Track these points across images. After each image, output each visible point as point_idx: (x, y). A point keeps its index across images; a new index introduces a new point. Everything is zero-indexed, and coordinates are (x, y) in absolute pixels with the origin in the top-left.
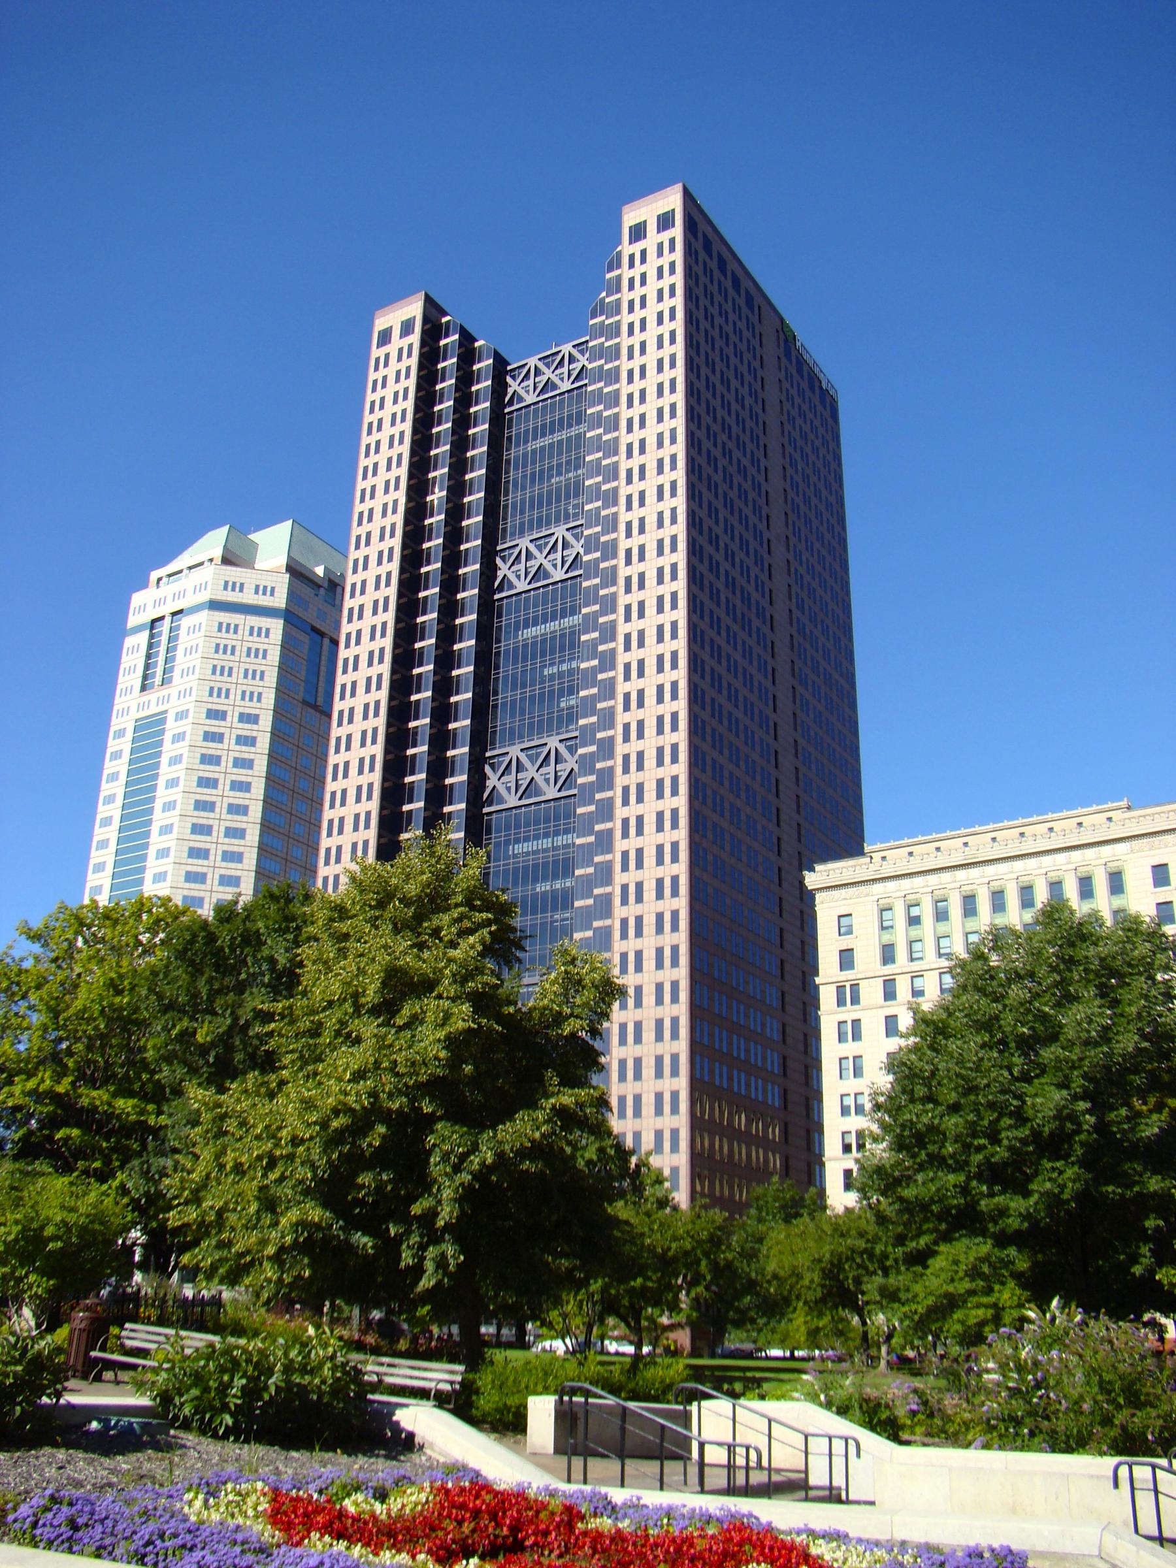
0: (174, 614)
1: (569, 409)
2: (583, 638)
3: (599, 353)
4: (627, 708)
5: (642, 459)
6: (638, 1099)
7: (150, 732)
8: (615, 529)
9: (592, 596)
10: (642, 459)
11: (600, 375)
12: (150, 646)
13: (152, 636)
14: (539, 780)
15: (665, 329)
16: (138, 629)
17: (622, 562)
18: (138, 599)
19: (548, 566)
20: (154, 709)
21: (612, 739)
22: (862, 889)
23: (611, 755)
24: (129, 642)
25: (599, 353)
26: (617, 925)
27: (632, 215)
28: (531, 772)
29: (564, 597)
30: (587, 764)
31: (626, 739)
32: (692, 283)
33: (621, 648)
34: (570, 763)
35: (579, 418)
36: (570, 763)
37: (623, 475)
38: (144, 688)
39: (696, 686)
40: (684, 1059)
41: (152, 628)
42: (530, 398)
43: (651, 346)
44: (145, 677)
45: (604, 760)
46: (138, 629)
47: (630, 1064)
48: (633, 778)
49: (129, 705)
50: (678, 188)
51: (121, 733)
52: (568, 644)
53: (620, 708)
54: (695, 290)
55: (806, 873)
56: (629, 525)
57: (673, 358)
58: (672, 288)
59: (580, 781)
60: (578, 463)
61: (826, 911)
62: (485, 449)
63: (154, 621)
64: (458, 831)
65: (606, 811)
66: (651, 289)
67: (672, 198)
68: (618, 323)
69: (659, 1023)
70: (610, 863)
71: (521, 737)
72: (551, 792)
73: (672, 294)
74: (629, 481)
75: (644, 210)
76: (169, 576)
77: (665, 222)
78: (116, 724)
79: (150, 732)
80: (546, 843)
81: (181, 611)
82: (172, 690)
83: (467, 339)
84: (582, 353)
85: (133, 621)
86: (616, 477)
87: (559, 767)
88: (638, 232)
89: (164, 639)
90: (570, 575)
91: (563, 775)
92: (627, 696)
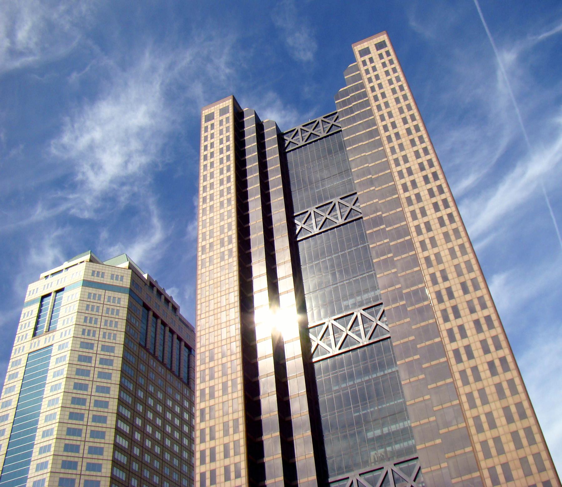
0: (58, 292)
12: (40, 311)
13: (41, 305)
15: (224, 156)
16: (32, 302)
18: (31, 287)
24: (25, 311)
27: (206, 111)
38: (34, 335)
44: (36, 329)
46: (32, 302)
49: (23, 345)
50: (231, 97)
51: (17, 363)
63: (43, 297)
64: (396, 345)
67: (227, 102)
75: (213, 108)
76: (53, 274)
77: (223, 111)
78: (14, 356)
79: (39, 359)
81: (62, 290)
82: (57, 334)
85: (27, 299)
88: (210, 117)
89: (50, 306)
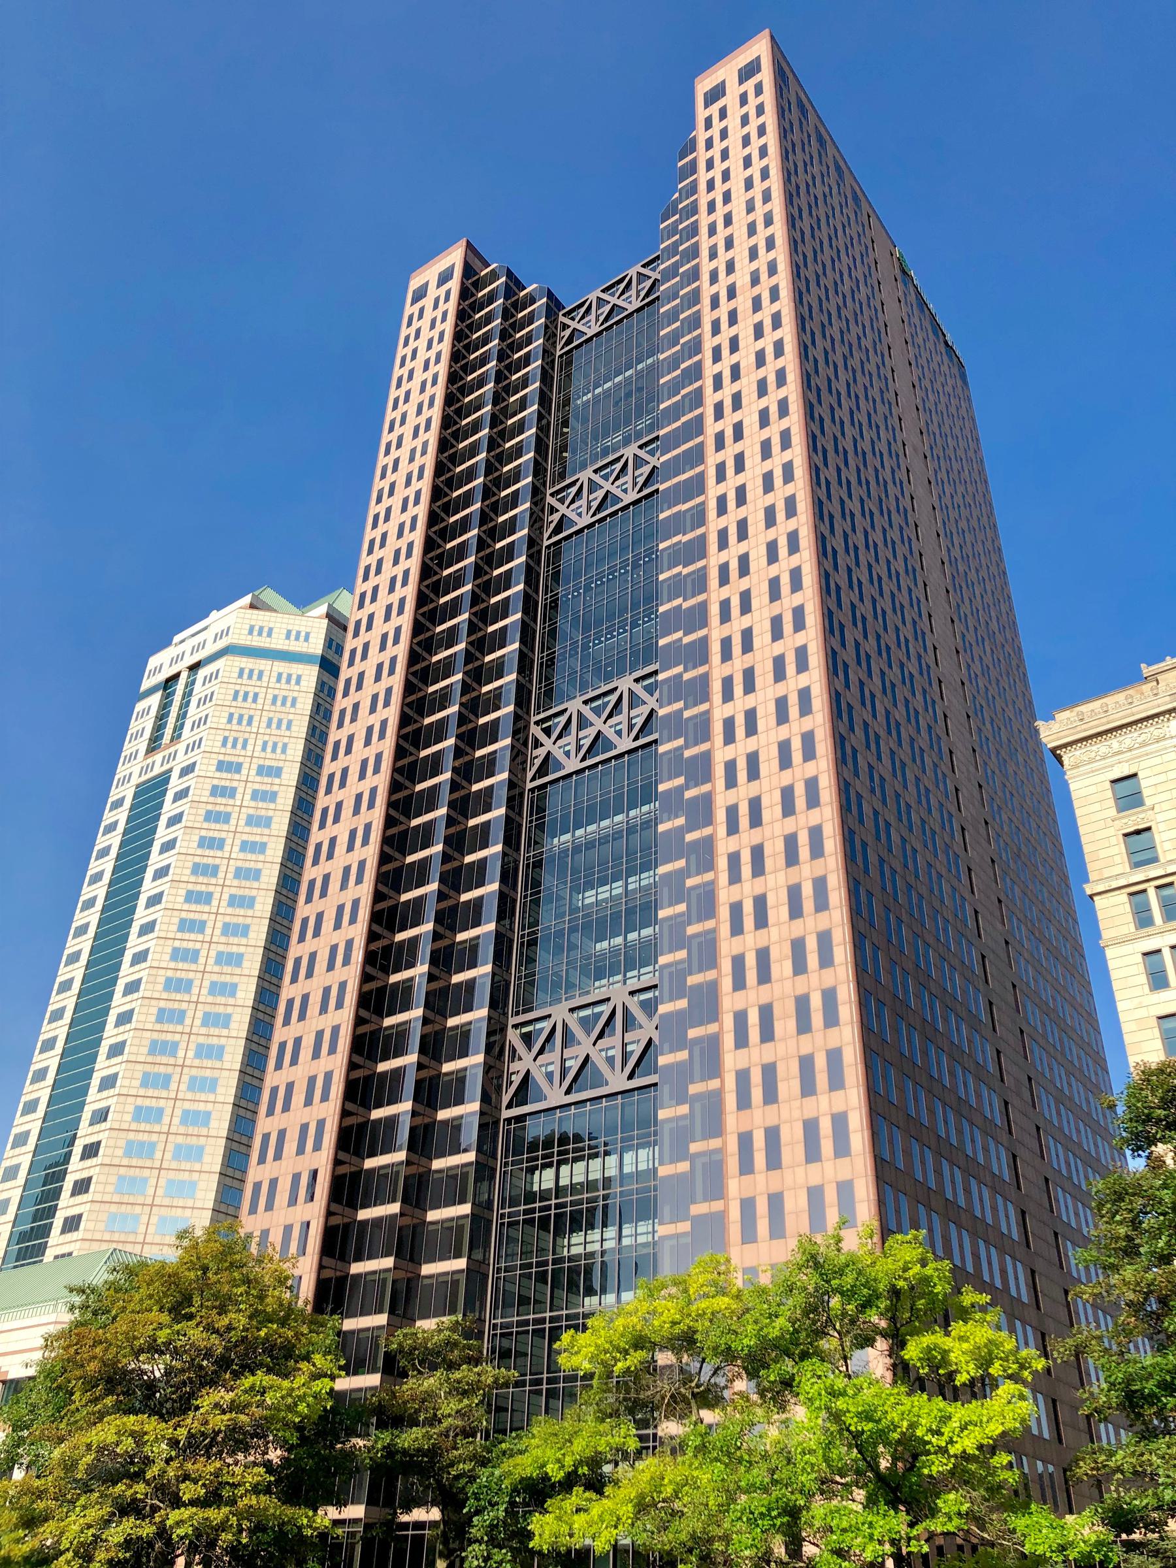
1: (637, 524)
2: (662, 642)
3: (678, 689)
4: (739, 983)
5: (751, 744)
6: (773, 1135)
7: (151, 794)
8: (709, 820)
9: (676, 846)
10: (751, 744)
11: (676, 725)
14: (598, 1059)
17: (722, 830)
18: (153, 662)
19: (609, 733)
20: (157, 770)
21: (714, 986)
22: (1151, 731)
23: (713, 1015)
24: (140, 706)
25: (678, 689)
26: (735, 1213)
28: (584, 1045)
29: (634, 772)
30: (675, 1028)
31: (739, 983)
32: (813, 398)
33: (725, 929)
34: (646, 1029)
35: (648, 794)
36: (646, 1029)
37: (719, 771)
39: (847, 784)
40: (847, 995)
41: (165, 689)
42: (572, 764)
43: (762, 636)
45: (701, 1024)
47: (756, 1077)
48: (752, 998)
50: (766, 32)
52: (641, 851)
53: (727, 983)
54: (838, 616)
55: (1040, 724)
56: (732, 811)
57: (808, 739)
58: (802, 654)
59: (662, 1060)
60: (648, 794)
61: (1087, 786)
62: (538, 397)
63: (168, 680)
65: (711, 1118)
66: (770, 785)
68: (704, 641)
69: (802, 1003)
70: (718, 1095)
71: (570, 986)
72: (618, 1081)
73: (802, 665)
74: (731, 782)
80: (618, 888)
83: (514, 283)
84: (650, 690)
86: (708, 777)
87: (629, 1037)
88: (717, 93)
90: (646, 492)
91: (636, 1049)
92: (738, 962)
